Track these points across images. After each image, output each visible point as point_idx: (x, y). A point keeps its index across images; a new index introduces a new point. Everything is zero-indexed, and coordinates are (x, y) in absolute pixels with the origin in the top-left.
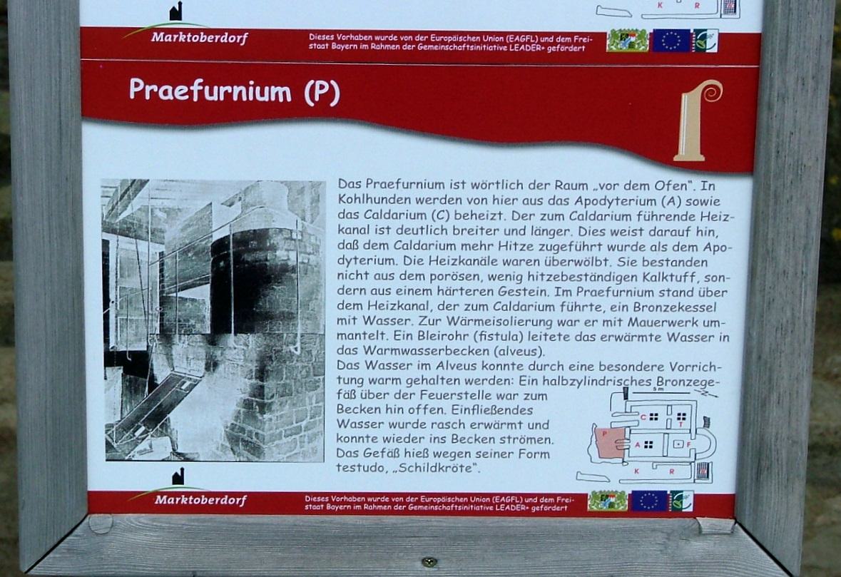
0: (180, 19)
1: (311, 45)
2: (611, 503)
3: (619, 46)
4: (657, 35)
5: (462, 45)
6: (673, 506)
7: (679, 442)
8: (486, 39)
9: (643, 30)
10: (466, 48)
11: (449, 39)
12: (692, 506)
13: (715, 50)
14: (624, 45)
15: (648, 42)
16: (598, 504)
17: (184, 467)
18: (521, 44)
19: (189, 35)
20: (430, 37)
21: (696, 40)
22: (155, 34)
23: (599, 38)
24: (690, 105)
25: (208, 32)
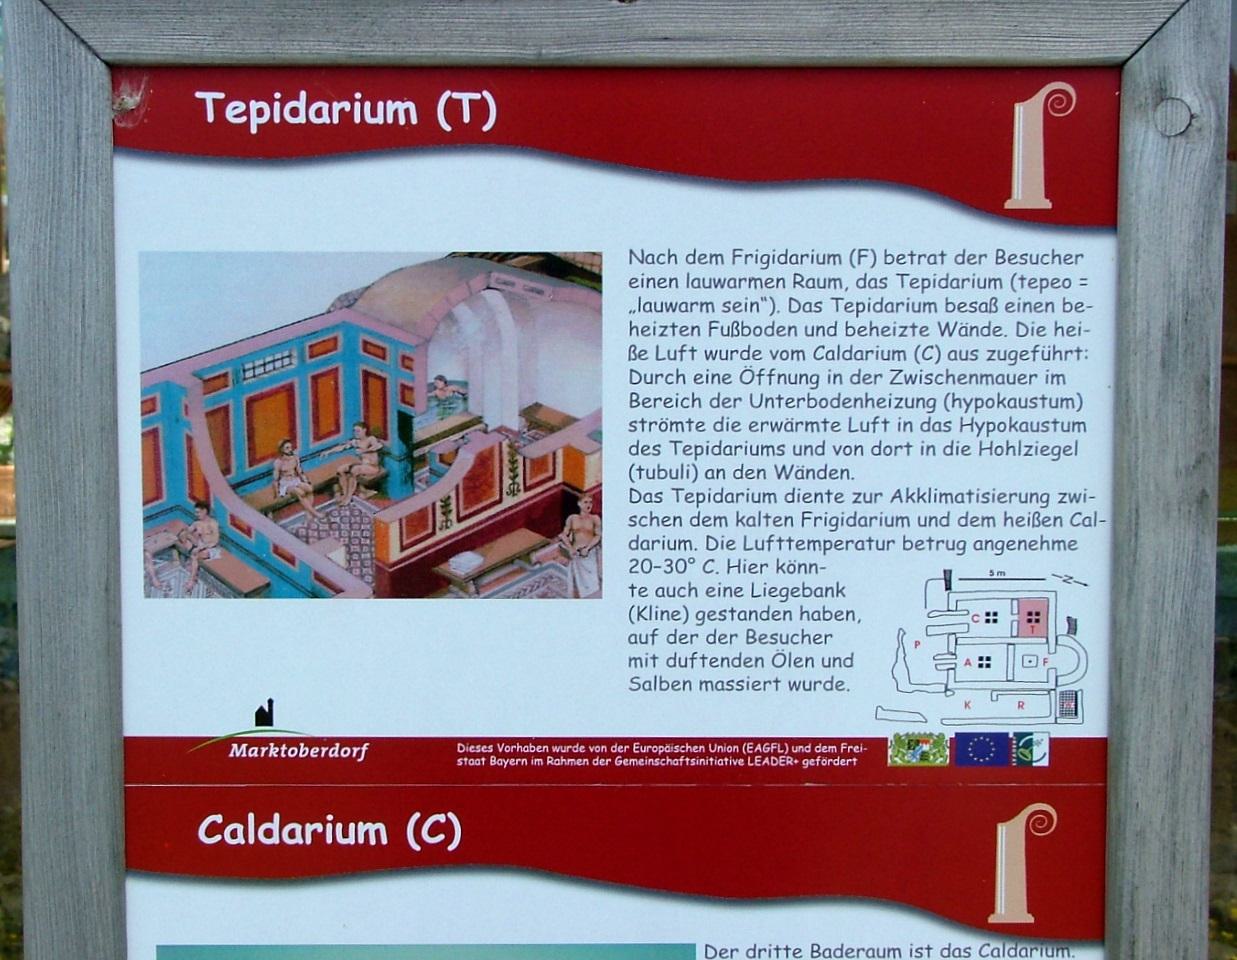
0: (271, 724)
1: (459, 760)
2: (923, 753)
3: (906, 758)
4: (961, 741)
5: (679, 758)
6: (1018, 758)
7: (1031, 664)
8: (713, 749)
9: (940, 734)
10: (684, 762)
11: (660, 749)
12: (1047, 756)
13: (1045, 762)
14: (913, 756)
15: (948, 752)
16: (904, 755)
17: (273, 698)
18: (764, 756)
19: (284, 748)
20: (632, 747)
21: (1018, 748)
22: (235, 746)
23: (877, 746)
24: (1010, 840)
25: (311, 742)
